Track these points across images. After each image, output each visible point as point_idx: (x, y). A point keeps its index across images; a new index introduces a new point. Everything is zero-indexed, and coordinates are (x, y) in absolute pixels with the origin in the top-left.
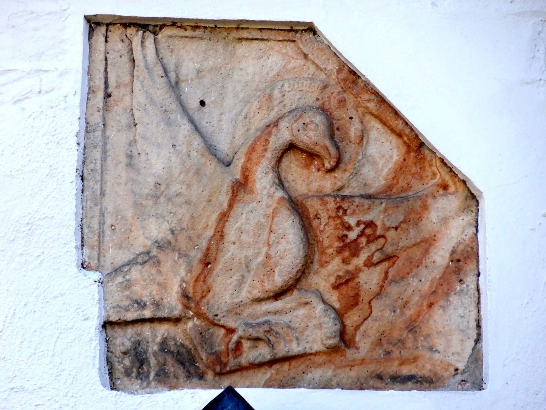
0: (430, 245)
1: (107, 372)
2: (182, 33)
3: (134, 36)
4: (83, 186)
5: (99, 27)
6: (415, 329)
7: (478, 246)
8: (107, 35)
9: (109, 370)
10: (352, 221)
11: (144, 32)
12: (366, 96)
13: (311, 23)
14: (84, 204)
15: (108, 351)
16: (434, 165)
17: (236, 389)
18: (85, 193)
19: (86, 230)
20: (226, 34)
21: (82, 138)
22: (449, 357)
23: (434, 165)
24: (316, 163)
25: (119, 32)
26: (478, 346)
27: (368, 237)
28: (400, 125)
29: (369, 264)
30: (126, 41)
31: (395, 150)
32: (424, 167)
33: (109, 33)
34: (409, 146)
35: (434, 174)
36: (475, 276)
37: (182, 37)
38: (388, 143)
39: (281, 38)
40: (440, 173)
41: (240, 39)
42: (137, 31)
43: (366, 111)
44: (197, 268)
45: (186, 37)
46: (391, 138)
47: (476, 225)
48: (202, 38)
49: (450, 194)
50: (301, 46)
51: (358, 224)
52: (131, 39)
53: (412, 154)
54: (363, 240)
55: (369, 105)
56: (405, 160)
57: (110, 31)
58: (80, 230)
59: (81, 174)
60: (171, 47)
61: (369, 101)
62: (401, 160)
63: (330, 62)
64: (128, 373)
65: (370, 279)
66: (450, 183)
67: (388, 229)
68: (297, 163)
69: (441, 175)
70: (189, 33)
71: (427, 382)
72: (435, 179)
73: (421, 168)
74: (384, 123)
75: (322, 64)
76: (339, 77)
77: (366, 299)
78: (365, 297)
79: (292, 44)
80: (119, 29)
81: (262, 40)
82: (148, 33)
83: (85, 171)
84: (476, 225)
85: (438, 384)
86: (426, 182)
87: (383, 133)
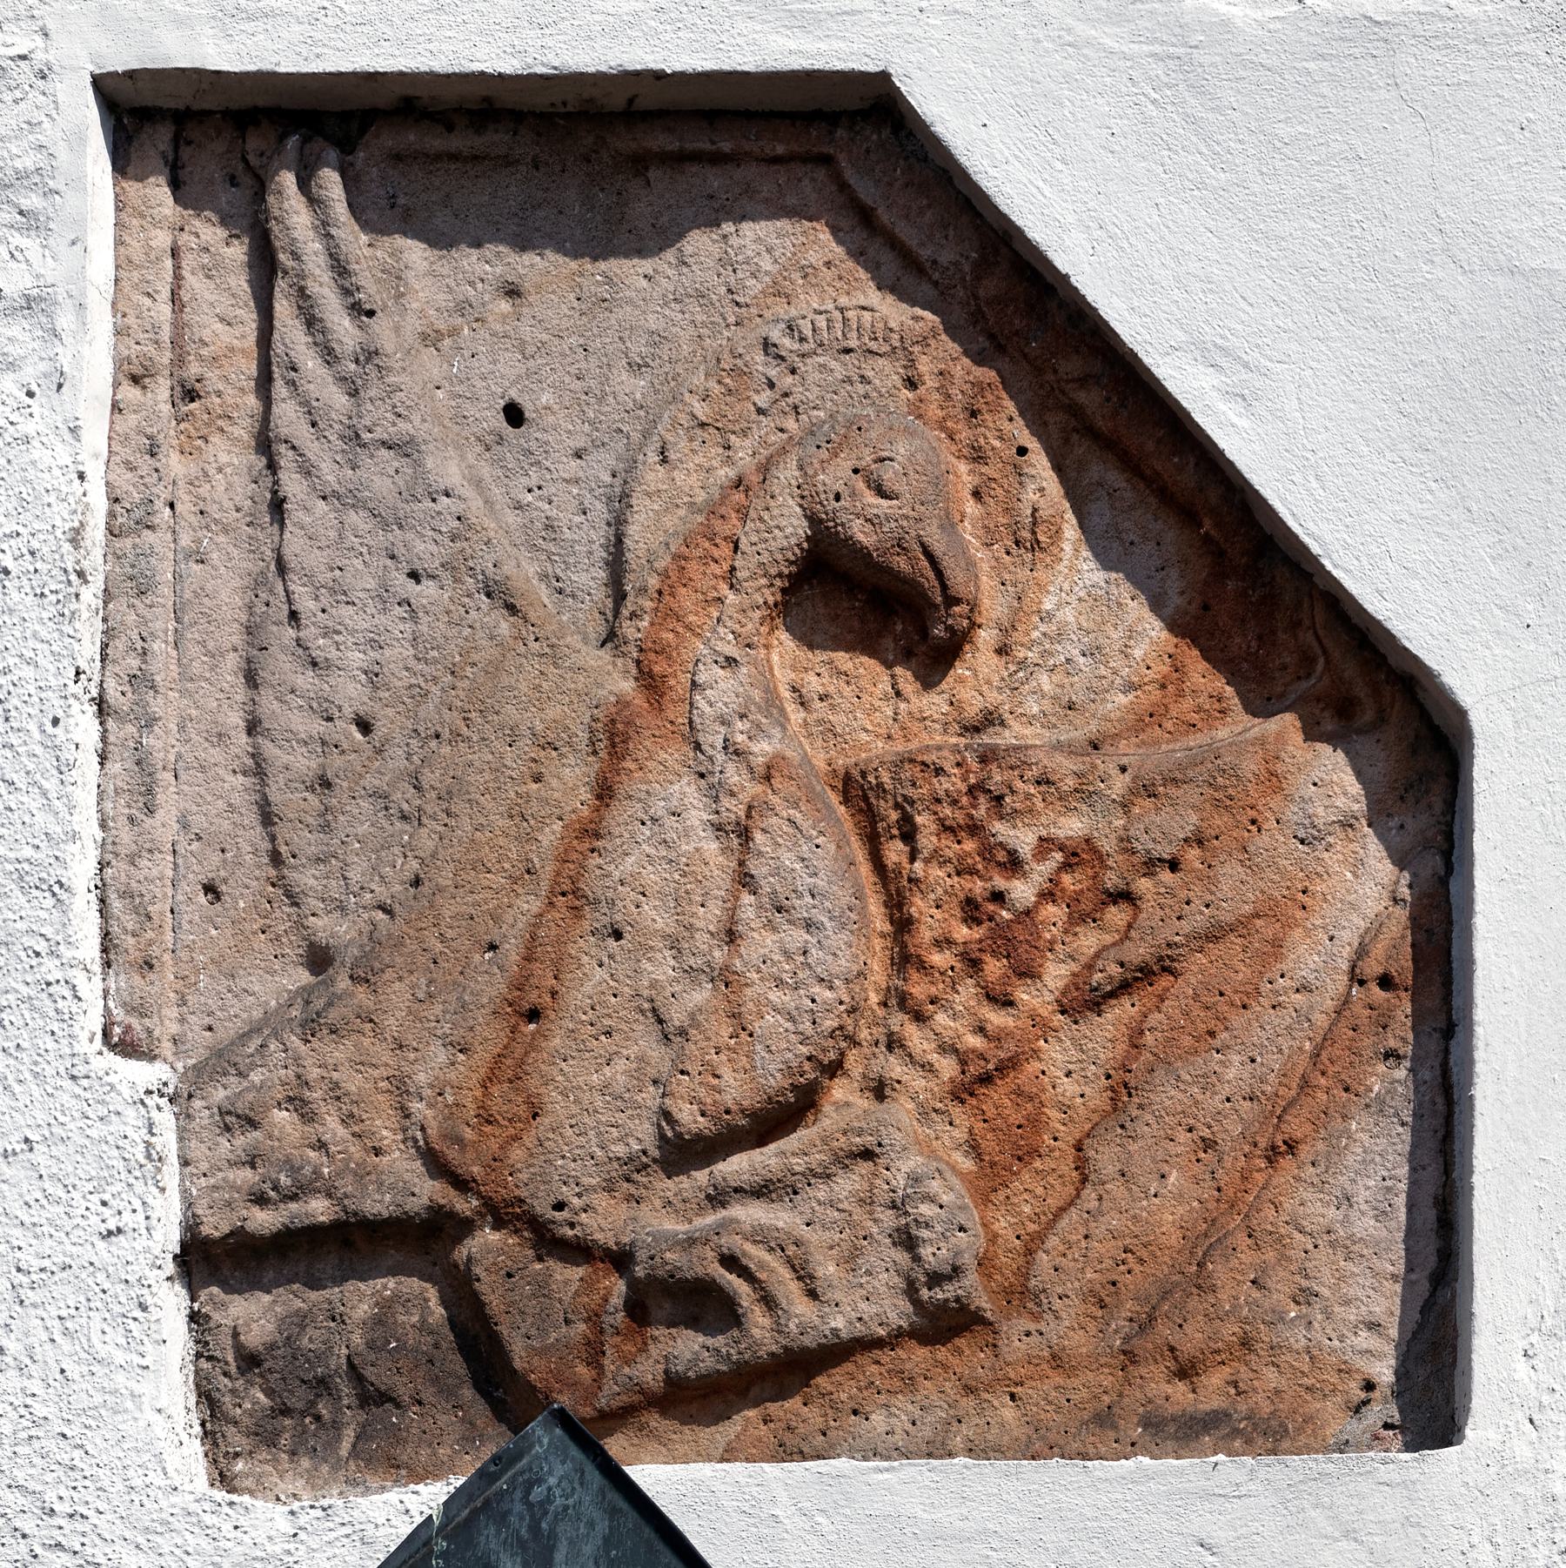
0: (1291, 924)
1: (197, 1429)
2: (437, 142)
3: (270, 158)
4: (104, 739)
5: (148, 129)
6: (1230, 1240)
7: (1450, 923)
8: (176, 159)
9: (203, 1424)
10: (1023, 839)
11: (305, 140)
12: (1071, 366)
13: (884, 76)
14: (108, 805)
15: (198, 1355)
16: (1307, 622)
17: (627, 1469)
18: (108, 765)
19: (116, 905)
20: (590, 140)
21: (97, 554)
22: (1341, 1339)
23: (1307, 622)
24: (899, 627)
25: (219, 146)
26: (1443, 1295)
27: (1074, 901)
28: (1186, 478)
29: (1084, 1001)
30: (247, 180)
31: (1174, 573)
32: (1273, 632)
33: (186, 153)
34: (1221, 554)
35: (1307, 660)
36: (1436, 1035)
37: (438, 157)
38: (1150, 546)
39: (780, 149)
40: (1325, 652)
41: (640, 163)
42: (282, 138)
43: (1073, 423)
44: (490, 1036)
45: (454, 157)
46: (1159, 525)
47: (1445, 846)
48: (508, 162)
49: (1359, 732)
50: (850, 176)
51: (1045, 845)
52: (261, 172)
53: (1231, 585)
54: (1054, 913)
55: (1082, 397)
56: (1206, 607)
57: (189, 143)
58: (95, 906)
59: (95, 693)
60: (401, 201)
61: (1083, 381)
62: (1193, 609)
63: (951, 233)
64: (264, 1437)
65: (1070, 1067)
66: (1361, 691)
67: (1150, 865)
68: (833, 630)
69: (1327, 662)
70: (458, 142)
71: (1267, 1433)
72: (1309, 676)
73: (1260, 638)
74: (1131, 464)
75: (923, 244)
76: (981, 293)
77: (1069, 1135)
78: (1060, 1130)
79: (821, 173)
80: (219, 134)
81: (716, 159)
82: (318, 144)
83: (111, 684)
84: (1445, 846)
85: (1303, 1440)
86: (1279, 689)
87: (1132, 508)
